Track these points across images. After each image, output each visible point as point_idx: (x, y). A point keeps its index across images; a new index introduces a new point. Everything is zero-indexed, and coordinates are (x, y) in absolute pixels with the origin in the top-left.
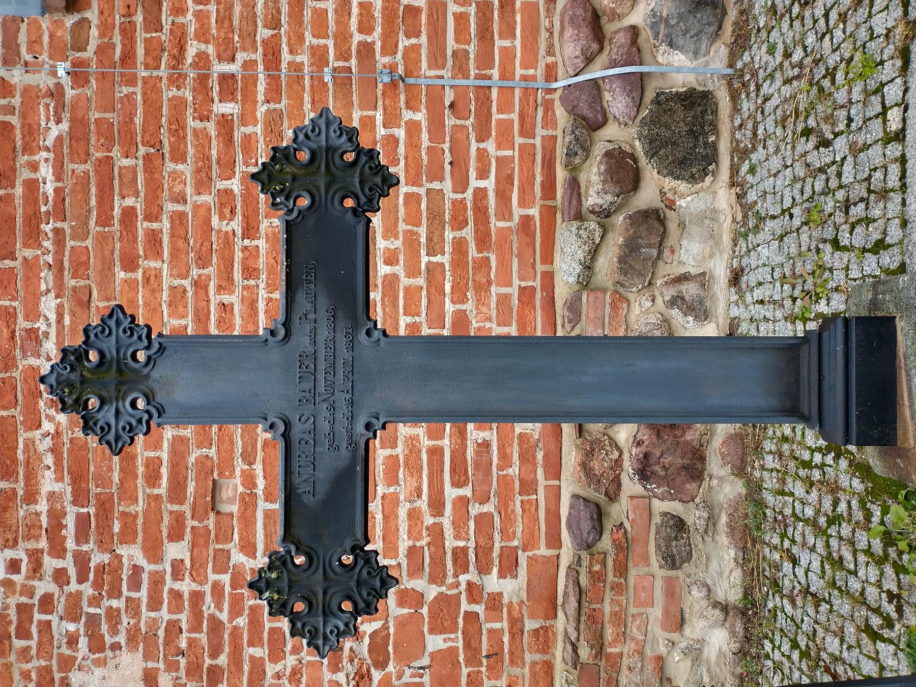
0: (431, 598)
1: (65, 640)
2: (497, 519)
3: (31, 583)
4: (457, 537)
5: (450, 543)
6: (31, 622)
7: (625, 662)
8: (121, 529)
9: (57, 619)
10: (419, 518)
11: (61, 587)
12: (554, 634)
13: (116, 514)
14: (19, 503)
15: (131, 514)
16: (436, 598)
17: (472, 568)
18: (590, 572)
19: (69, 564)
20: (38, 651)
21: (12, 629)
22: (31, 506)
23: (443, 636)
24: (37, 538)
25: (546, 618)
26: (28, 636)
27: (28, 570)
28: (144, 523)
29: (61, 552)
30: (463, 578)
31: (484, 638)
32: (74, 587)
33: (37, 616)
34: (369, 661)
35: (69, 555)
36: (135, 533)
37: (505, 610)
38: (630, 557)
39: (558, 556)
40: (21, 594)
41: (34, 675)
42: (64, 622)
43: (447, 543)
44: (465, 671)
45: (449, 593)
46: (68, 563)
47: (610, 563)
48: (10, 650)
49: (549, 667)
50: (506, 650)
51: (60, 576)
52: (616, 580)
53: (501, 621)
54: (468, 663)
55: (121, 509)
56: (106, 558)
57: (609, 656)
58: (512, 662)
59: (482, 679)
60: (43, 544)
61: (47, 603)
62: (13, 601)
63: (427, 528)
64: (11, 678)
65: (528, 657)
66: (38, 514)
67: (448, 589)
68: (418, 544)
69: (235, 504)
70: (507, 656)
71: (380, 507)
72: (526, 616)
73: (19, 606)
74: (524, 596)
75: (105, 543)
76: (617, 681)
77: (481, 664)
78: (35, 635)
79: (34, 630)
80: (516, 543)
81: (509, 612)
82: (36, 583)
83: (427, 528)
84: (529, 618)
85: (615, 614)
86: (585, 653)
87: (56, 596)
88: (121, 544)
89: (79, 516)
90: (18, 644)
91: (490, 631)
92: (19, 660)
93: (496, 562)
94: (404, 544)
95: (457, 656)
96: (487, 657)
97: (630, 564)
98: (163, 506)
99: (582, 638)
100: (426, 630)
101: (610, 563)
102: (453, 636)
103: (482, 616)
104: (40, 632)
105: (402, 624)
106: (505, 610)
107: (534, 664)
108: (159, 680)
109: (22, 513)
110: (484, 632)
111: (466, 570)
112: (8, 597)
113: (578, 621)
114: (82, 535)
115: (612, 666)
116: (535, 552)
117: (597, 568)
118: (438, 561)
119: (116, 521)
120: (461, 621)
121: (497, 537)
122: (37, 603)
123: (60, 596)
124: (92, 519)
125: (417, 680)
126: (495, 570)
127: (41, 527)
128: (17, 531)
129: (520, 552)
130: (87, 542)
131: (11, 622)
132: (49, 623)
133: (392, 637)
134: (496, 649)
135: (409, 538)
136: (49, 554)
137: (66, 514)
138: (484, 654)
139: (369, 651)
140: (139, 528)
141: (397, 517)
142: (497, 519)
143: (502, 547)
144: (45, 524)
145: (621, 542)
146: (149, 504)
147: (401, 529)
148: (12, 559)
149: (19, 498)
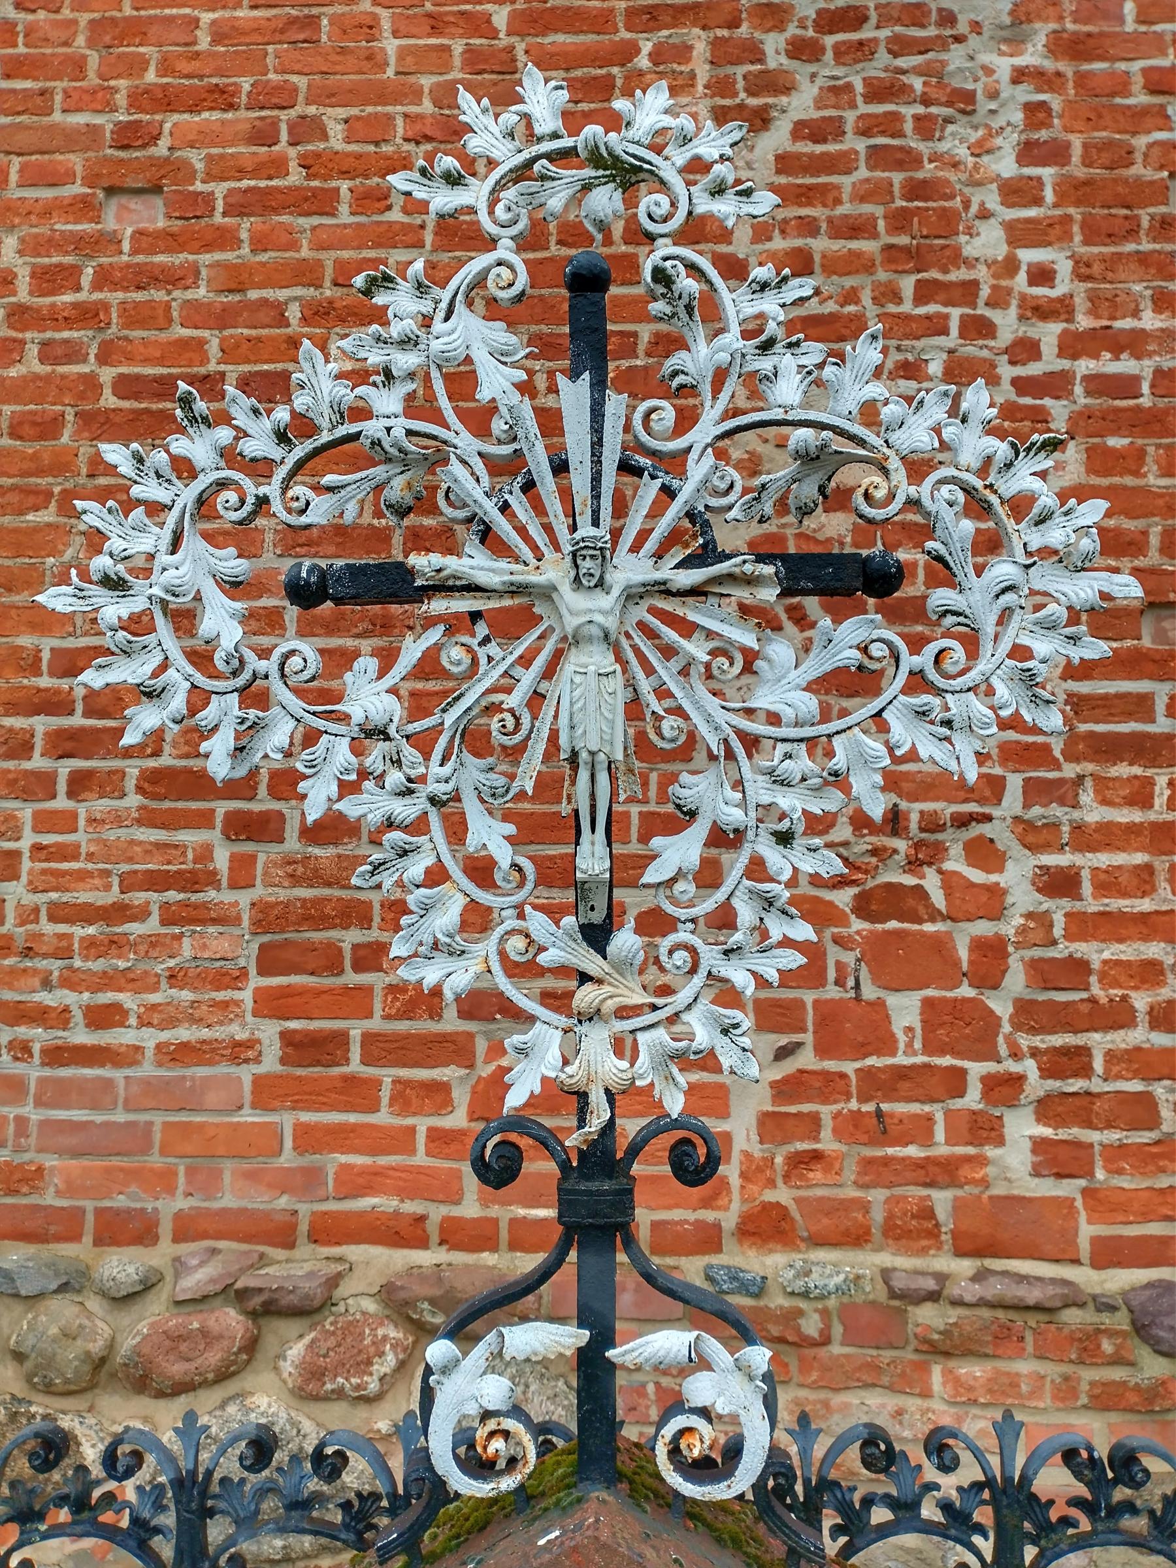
0: (991, 1004)
1: (910, 358)
2: (1146, 1137)
3: (1014, 303)
4: (1111, 1057)
5: (1099, 1042)
6: (945, 305)
7: (912, 1404)
8: (1112, 451)
9: (951, 345)
10: (1144, 981)
11: (1006, 351)
12: (923, 1251)
13: (1140, 442)
14: (1155, 284)
15: (1141, 466)
16: (992, 1012)
17: (1053, 1085)
18: (1098, 1331)
19: (1048, 363)
20: (893, 316)
21: (934, 274)
22: (1149, 304)
23: (918, 1027)
24: (1094, 312)
25: (955, 1234)
26: (919, 300)
27: (1037, 297)
28: (1125, 488)
29: (1071, 351)
30: (1030, 1067)
31: (915, 1108)
32: (1007, 372)
33: (955, 313)
34: (870, 884)
35: (1065, 364)
36: (1106, 473)
37: (971, 1150)
38: (1129, 1417)
39: (1076, 1262)
40: (994, 288)
41: (851, 309)
42: (945, 356)
43: (1097, 1036)
44: (849, 1067)
45: (1000, 1039)
46: (1049, 362)
47: (1117, 1374)
48: (896, 272)
49: (857, 1238)
50: (890, 1151)
51: (1025, 350)
52: (1084, 1387)
53: (947, 1143)
54: (866, 1075)
55: (1151, 450)
56: (1060, 424)
57: (923, 1368)
58: (868, 1164)
59: (835, 1102)
60: (1083, 322)
61: (979, 328)
62: (981, 273)
63: (1124, 998)
64: (849, 274)
65: (877, 1196)
66: (1136, 313)
67: (1007, 1037)
68: (1093, 979)
69: (1154, 642)
70: (879, 1152)
71: (1164, 908)
72: (959, 1193)
73: (974, 284)
74: (998, 1190)
75: (1081, 423)
76: (874, 1385)
77: (863, 1099)
78: (922, 310)
79: (931, 308)
80: (1100, 1174)
81: (968, 1159)
82: (1013, 311)
83: (1124, 998)
84: (956, 1199)
85: (1013, 1382)
86: (928, 1316)
87: (992, 343)
88: (1087, 450)
89: (1136, 380)
90: (907, 284)
91: (929, 1119)
92: (876, 286)
93: (1063, 1134)
94: (1097, 953)
95: (879, 1053)
96: (879, 1114)
97: (1114, 1417)
98: (1157, 519)
99: (961, 1311)
100: (930, 992)
101: (1117, 1374)
102: (918, 1045)
103: (957, 1104)
104: (928, 317)
105: (941, 946)
106: (971, 1150)
107: (865, 1207)
108: (839, 514)
109: (1137, 288)
110: (927, 1108)
111: (1047, 1073)
112: (989, 266)
113: (992, 1305)
114: (1098, 384)
115: (903, 1375)
116: (1083, 1217)
117: (1107, 1346)
118: (1063, 1018)
119: (1127, 441)
120: (946, 1061)
121: (1113, 1136)
122: (979, 312)
123: (991, 349)
124: (1131, 402)
125: (831, 974)
126: (1047, 1132)
127: (1113, 318)
128: (1104, 280)
129: (1082, 1183)
130: (1088, 393)
131: (946, 271)
132: (945, 332)
133: (916, 927)
134: (894, 1130)
135: (1105, 962)
136: (1065, 332)
137: (1138, 358)
138: (885, 1107)
139: (889, 885)
140: (1116, 480)
141: (1146, 938)
142: (1146, 1137)
143: (1091, 1145)
144: (1119, 324)
145: (1163, 1398)
146: (1161, 496)
147: (1122, 947)
148: (1055, 272)
149: (1163, 284)
